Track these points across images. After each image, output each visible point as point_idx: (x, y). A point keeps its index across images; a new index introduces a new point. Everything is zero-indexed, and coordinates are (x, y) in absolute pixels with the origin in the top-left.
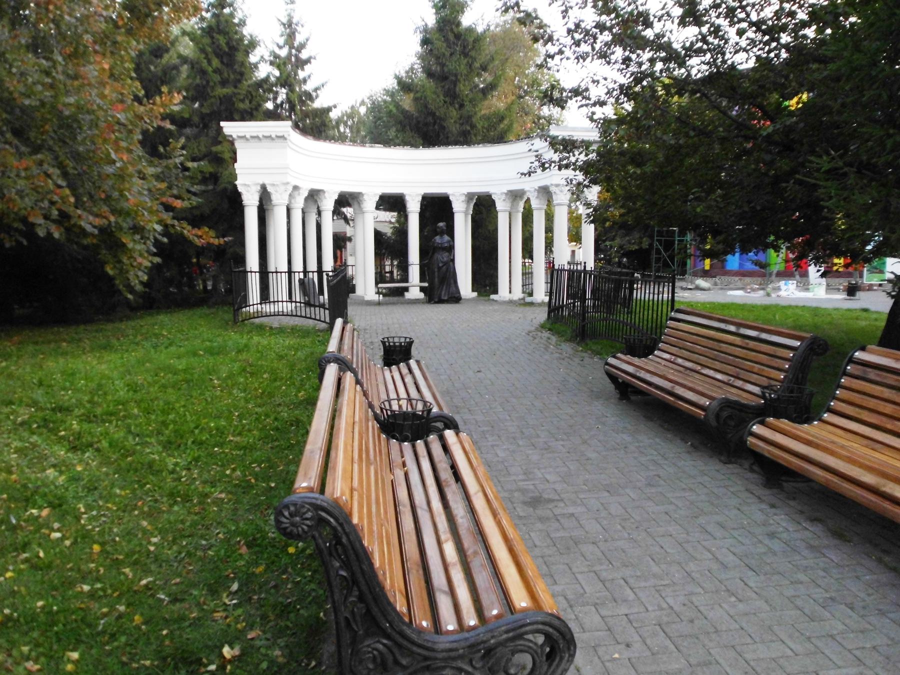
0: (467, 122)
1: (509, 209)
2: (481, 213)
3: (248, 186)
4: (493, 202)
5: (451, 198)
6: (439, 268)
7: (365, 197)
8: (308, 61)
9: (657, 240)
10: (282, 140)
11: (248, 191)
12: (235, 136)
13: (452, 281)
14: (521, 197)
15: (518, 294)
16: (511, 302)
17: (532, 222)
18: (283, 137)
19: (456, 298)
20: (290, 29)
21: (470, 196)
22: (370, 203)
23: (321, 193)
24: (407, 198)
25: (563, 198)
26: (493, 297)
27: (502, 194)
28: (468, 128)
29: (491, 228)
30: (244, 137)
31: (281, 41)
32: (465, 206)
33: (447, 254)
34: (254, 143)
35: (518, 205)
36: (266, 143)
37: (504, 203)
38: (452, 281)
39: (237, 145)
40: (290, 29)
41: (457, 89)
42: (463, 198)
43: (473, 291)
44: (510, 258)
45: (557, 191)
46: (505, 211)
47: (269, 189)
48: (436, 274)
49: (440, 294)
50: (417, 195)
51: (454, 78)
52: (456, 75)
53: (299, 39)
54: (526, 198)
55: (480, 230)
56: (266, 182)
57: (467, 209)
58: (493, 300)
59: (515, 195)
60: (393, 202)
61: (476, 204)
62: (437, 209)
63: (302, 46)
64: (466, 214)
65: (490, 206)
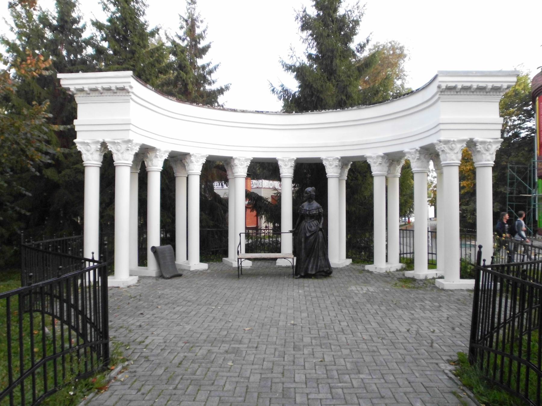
0: (343, 92)
1: (385, 173)
2: (356, 179)
3: (87, 144)
4: (369, 166)
5: (324, 163)
6: (307, 238)
7: (236, 162)
8: (204, 50)
9: (509, 205)
10: (123, 93)
11: (88, 151)
12: (72, 88)
13: (321, 253)
14: (398, 161)
15: (395, 265)
16: (388, 275)
17: (493, 176)
18: (123, 89)
19: (325, 272)
20: (191, 25)
21: (344, 161)
22: (241, 170)
23: (188, 157)
24: (280, 163)
25: (454, 157)
26: (368, 267)
27: (378, 157)
28: (344, 98)
29: (367, 194)
30: (82, 90)
31: (181, 33)
32: (339, 171)
33: (315, 222)
34: (94, 97)
35: (395, 169)
36: (108, 97)
37: (379, 168)
38: (321, 253)
39: (78, 99)
40: (191, 25)
41: (334, 64)
42: (337, 163)
43: (348, 257)
44: (387, 229)
45: (447, 150)
46: (381, 175)
47: (111, 147)
48: (303, 245)
49: (307, 268)
50: (290, 160)
51: (330, 54)
52: (332, 51)
53: (198, 31)
54: (403, 162)
55: (356, 196)
56: (107, 140)
57: (341, 174)
58: (368, 271)
59: (392, 159)
60: (265, 169)
61: (350, 171)
62: (310, 174)
63: (201, 36)
64: (340, 178)
65: (366, 172)
